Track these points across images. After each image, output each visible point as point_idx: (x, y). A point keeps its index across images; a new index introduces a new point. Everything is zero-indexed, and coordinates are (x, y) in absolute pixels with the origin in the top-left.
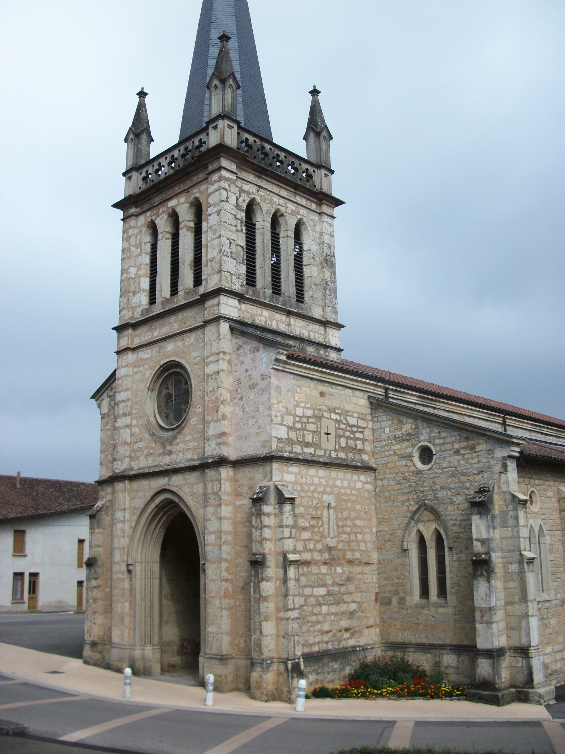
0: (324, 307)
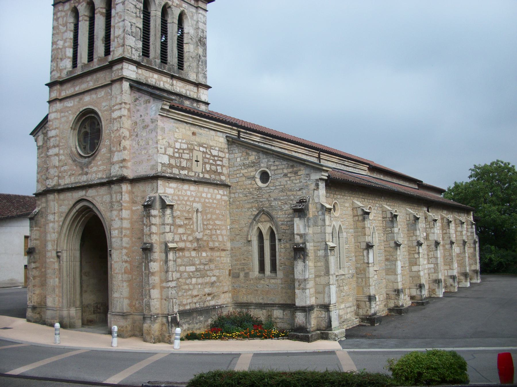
0: (197, 73)
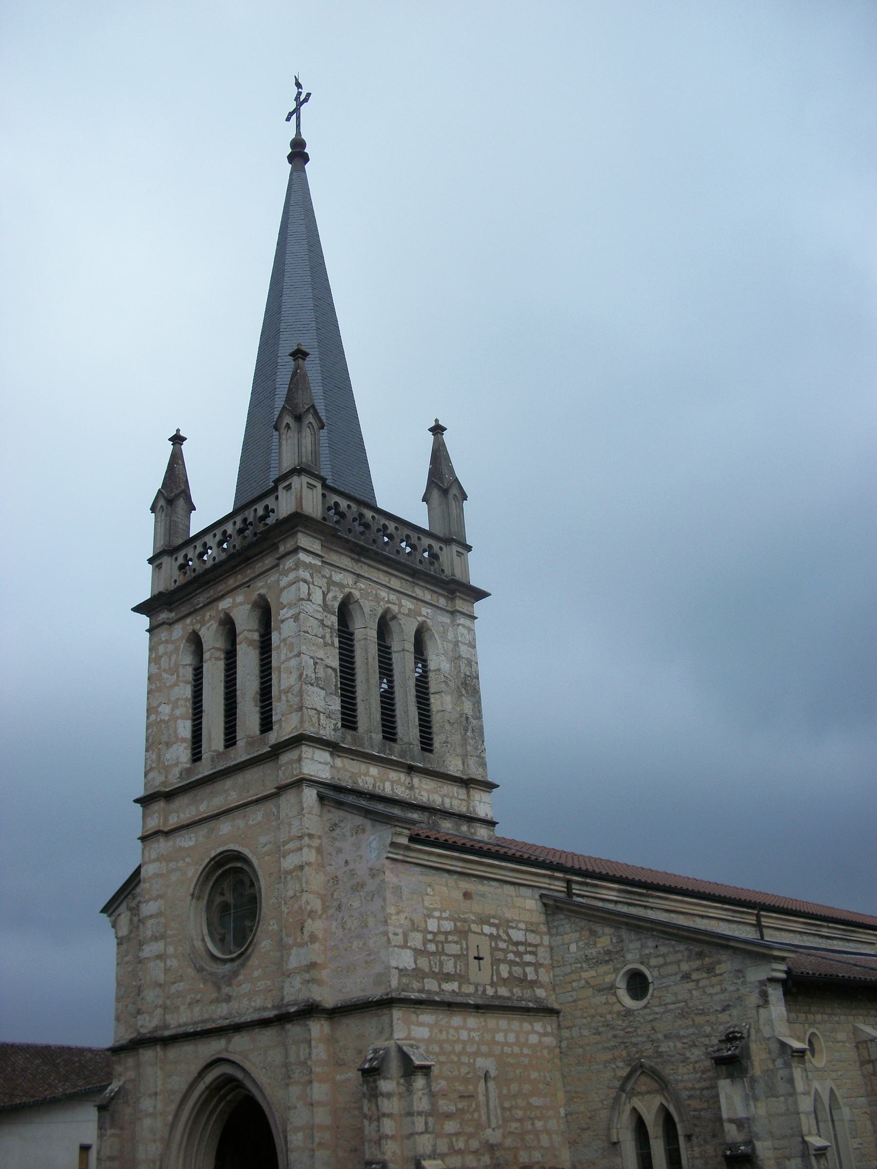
0: (464, 757)
